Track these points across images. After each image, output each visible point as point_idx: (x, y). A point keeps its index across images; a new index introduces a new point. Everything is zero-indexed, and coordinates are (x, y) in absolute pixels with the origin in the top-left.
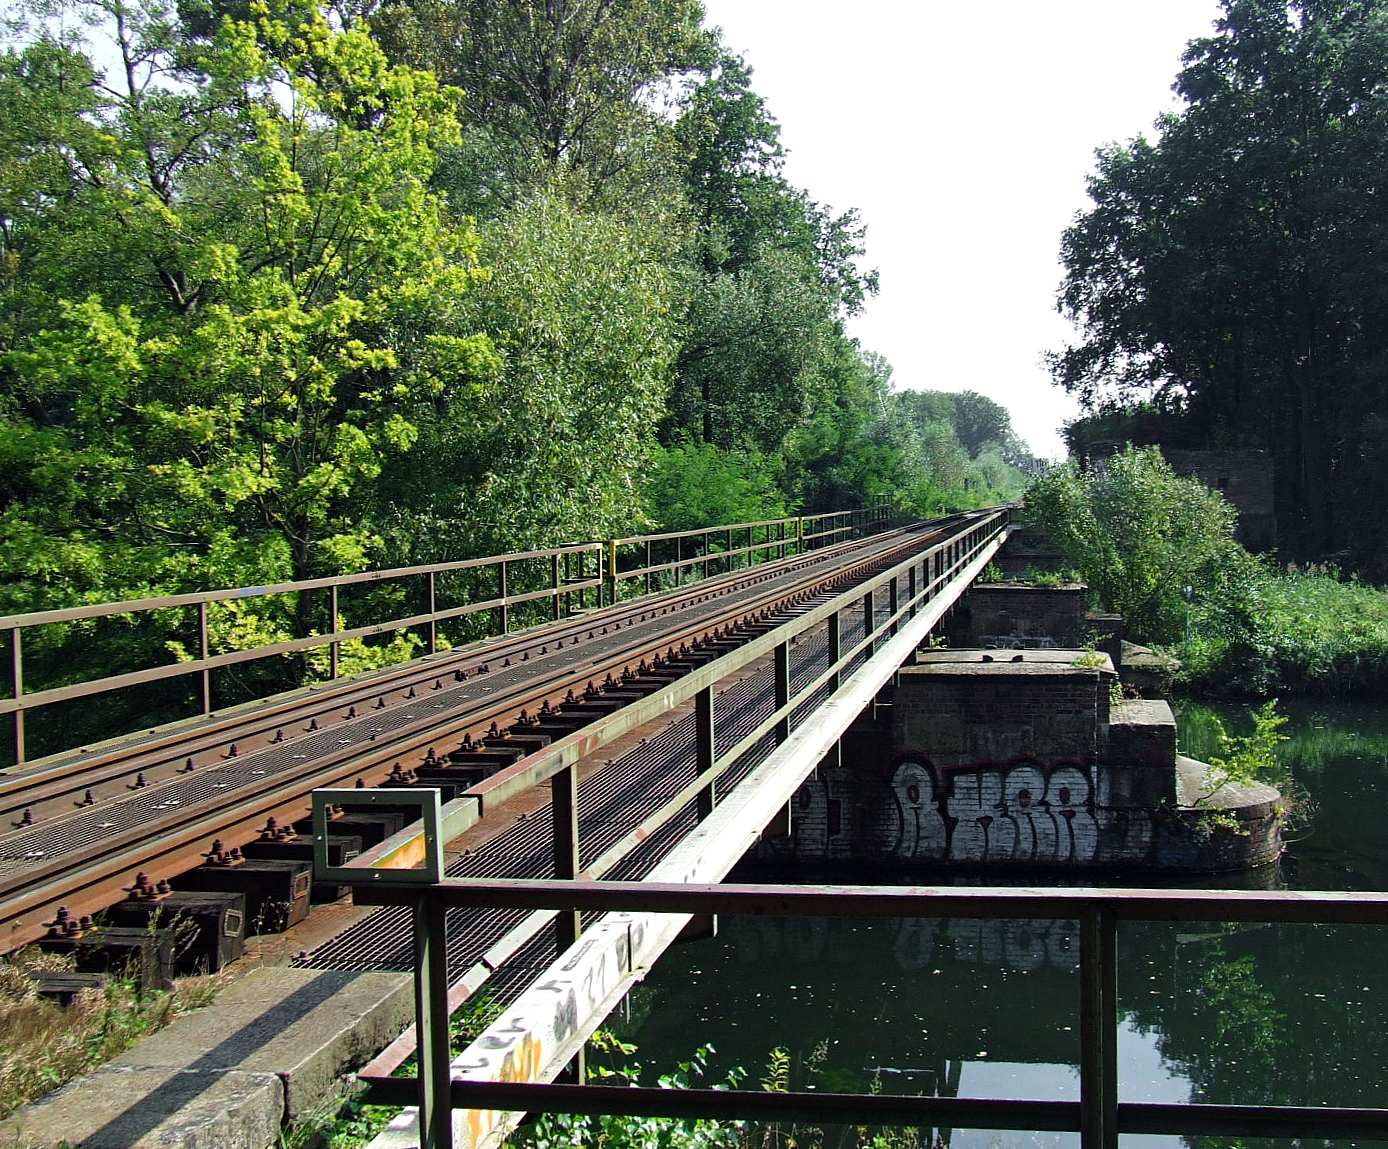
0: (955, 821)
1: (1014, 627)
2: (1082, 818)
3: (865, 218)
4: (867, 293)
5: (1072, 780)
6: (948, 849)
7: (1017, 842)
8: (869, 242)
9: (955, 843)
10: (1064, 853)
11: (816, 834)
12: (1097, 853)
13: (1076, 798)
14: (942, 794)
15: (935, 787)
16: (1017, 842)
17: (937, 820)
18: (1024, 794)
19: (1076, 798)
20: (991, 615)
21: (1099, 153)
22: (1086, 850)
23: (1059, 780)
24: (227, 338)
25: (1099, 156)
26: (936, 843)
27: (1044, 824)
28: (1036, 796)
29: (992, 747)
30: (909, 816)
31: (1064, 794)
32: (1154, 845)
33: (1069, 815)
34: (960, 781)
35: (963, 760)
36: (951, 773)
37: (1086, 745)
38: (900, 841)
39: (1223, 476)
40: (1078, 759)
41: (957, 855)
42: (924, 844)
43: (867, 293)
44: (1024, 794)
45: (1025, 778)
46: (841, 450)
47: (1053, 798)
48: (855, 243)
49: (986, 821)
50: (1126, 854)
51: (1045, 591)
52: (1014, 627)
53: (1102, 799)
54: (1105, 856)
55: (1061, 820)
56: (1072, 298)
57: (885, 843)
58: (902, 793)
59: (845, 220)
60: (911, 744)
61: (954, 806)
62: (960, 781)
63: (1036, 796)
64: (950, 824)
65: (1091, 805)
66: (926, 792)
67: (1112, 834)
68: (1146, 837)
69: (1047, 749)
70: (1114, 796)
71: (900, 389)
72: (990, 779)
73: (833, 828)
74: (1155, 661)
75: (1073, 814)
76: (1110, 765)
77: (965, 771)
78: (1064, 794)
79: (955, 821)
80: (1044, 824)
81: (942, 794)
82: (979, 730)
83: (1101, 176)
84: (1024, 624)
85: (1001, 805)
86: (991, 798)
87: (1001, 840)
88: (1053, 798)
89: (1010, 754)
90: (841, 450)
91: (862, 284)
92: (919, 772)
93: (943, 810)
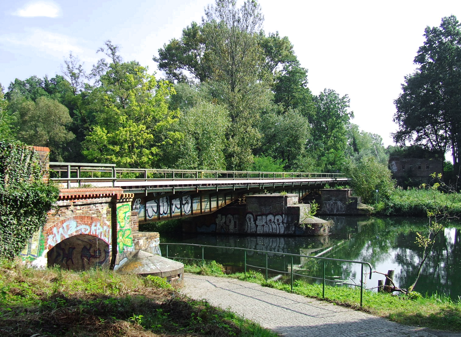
0: (258, 225)
1: (331, 199)
2: (281, 225)
3: (350, 96)
4: (351, 118)
5: (279, 217)
6: (256, 231)
7: (269, 230)
8: (351, 104)
9: (258, 230)
10: (278, 232)
11: (232, 228)
12: (284, 232)
13: (280, 221)
14: (255, 220)
15: (254, 219)
16: (269, 230)
17: (254, 225)
18: (270, 220)
19: (280, 221)
20: (326, 196)
21: (405, 77)
22: (282, 231)
23: (277, 217)
24: (123, 133)
25: (406, 78)
26: (254, 230)
27: (274, 226)
28: (273, 220)
29: (264, 211)
30: (249, 224)
31: (278, 220)
32: (295, 231)
33: (279, 224)
34: (259, 217)
35: (259, 213)
36: (257, 216)
37: (282, 210)
38: (247, 230)
39: (428, 165)
40: (280, 213)
41: (258, 232)
42: (252, 230)
43: (351, 118)
44: (270, 220)
45: (271, 217)
46: (335, 161)
47: (276, 221)
48: (347, 104)
49: (263, 225)
50: (290, 232)
51: (339, 191)
52: (331, 199)
53: (285, 221)
54: (286, 233)
55: (277, 225)
56: (398, 118)
57: (245, 230)
58: (248, 220)
59: (343, 98)
60: (250, 210)
61: (257, 223)
62: (259, 217)
63: (273, 220)
64: (257, 226)
65: (283, 222)
66: (252, 220)
67: (287, 228)
68: (293, 229)
69: (275, 211)
70: (287, 221)
71: (386, 147)
72: (264, 217)
73: (235, 227)
74: (366, 208)
75: (279, 224)
76: (287, 214)
77: (259, 215)
78: (278, 220)
79: (258, 225)
80: (274, 226)
81: (255, 220)
82: (262, 207)
83: (406, 84)
84: (334, 198)
85: (266, 222)
86: (264, 221)
87: (266, 229)
88: (276, 221)
89: (268, 212)
90: (335, 161)
91: (349, 115)
92: (251, 216)
93: (255, 223)
